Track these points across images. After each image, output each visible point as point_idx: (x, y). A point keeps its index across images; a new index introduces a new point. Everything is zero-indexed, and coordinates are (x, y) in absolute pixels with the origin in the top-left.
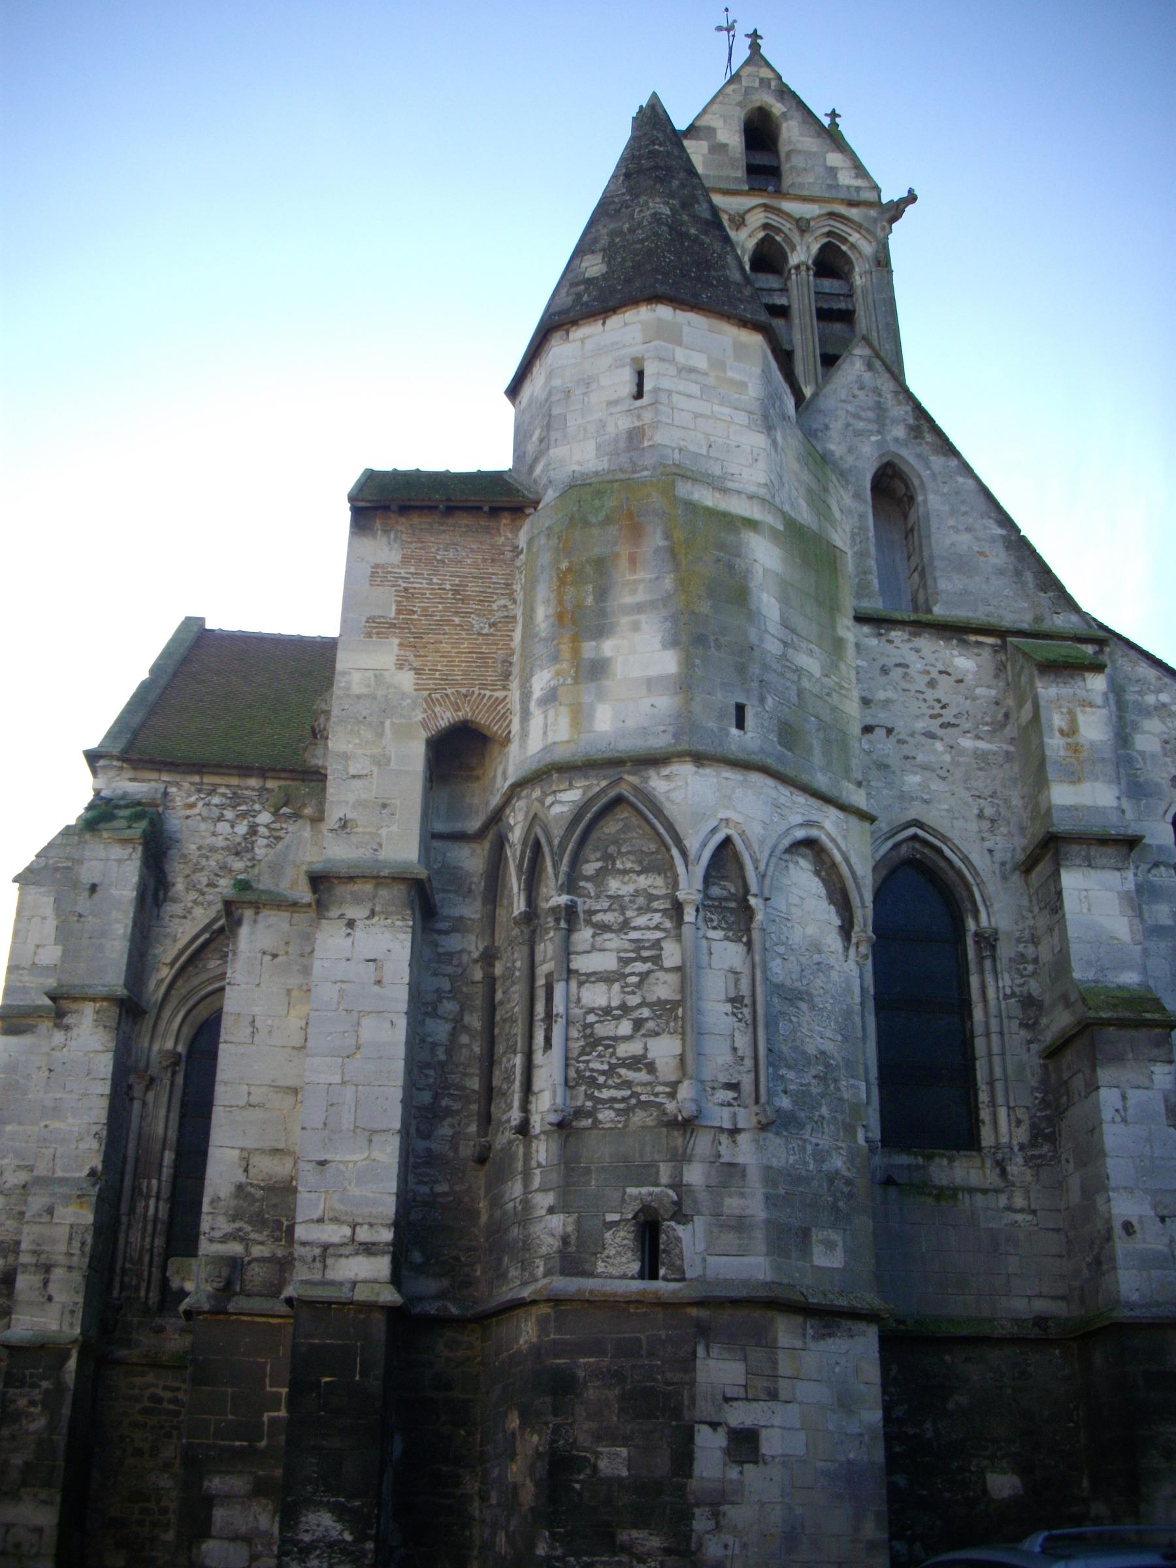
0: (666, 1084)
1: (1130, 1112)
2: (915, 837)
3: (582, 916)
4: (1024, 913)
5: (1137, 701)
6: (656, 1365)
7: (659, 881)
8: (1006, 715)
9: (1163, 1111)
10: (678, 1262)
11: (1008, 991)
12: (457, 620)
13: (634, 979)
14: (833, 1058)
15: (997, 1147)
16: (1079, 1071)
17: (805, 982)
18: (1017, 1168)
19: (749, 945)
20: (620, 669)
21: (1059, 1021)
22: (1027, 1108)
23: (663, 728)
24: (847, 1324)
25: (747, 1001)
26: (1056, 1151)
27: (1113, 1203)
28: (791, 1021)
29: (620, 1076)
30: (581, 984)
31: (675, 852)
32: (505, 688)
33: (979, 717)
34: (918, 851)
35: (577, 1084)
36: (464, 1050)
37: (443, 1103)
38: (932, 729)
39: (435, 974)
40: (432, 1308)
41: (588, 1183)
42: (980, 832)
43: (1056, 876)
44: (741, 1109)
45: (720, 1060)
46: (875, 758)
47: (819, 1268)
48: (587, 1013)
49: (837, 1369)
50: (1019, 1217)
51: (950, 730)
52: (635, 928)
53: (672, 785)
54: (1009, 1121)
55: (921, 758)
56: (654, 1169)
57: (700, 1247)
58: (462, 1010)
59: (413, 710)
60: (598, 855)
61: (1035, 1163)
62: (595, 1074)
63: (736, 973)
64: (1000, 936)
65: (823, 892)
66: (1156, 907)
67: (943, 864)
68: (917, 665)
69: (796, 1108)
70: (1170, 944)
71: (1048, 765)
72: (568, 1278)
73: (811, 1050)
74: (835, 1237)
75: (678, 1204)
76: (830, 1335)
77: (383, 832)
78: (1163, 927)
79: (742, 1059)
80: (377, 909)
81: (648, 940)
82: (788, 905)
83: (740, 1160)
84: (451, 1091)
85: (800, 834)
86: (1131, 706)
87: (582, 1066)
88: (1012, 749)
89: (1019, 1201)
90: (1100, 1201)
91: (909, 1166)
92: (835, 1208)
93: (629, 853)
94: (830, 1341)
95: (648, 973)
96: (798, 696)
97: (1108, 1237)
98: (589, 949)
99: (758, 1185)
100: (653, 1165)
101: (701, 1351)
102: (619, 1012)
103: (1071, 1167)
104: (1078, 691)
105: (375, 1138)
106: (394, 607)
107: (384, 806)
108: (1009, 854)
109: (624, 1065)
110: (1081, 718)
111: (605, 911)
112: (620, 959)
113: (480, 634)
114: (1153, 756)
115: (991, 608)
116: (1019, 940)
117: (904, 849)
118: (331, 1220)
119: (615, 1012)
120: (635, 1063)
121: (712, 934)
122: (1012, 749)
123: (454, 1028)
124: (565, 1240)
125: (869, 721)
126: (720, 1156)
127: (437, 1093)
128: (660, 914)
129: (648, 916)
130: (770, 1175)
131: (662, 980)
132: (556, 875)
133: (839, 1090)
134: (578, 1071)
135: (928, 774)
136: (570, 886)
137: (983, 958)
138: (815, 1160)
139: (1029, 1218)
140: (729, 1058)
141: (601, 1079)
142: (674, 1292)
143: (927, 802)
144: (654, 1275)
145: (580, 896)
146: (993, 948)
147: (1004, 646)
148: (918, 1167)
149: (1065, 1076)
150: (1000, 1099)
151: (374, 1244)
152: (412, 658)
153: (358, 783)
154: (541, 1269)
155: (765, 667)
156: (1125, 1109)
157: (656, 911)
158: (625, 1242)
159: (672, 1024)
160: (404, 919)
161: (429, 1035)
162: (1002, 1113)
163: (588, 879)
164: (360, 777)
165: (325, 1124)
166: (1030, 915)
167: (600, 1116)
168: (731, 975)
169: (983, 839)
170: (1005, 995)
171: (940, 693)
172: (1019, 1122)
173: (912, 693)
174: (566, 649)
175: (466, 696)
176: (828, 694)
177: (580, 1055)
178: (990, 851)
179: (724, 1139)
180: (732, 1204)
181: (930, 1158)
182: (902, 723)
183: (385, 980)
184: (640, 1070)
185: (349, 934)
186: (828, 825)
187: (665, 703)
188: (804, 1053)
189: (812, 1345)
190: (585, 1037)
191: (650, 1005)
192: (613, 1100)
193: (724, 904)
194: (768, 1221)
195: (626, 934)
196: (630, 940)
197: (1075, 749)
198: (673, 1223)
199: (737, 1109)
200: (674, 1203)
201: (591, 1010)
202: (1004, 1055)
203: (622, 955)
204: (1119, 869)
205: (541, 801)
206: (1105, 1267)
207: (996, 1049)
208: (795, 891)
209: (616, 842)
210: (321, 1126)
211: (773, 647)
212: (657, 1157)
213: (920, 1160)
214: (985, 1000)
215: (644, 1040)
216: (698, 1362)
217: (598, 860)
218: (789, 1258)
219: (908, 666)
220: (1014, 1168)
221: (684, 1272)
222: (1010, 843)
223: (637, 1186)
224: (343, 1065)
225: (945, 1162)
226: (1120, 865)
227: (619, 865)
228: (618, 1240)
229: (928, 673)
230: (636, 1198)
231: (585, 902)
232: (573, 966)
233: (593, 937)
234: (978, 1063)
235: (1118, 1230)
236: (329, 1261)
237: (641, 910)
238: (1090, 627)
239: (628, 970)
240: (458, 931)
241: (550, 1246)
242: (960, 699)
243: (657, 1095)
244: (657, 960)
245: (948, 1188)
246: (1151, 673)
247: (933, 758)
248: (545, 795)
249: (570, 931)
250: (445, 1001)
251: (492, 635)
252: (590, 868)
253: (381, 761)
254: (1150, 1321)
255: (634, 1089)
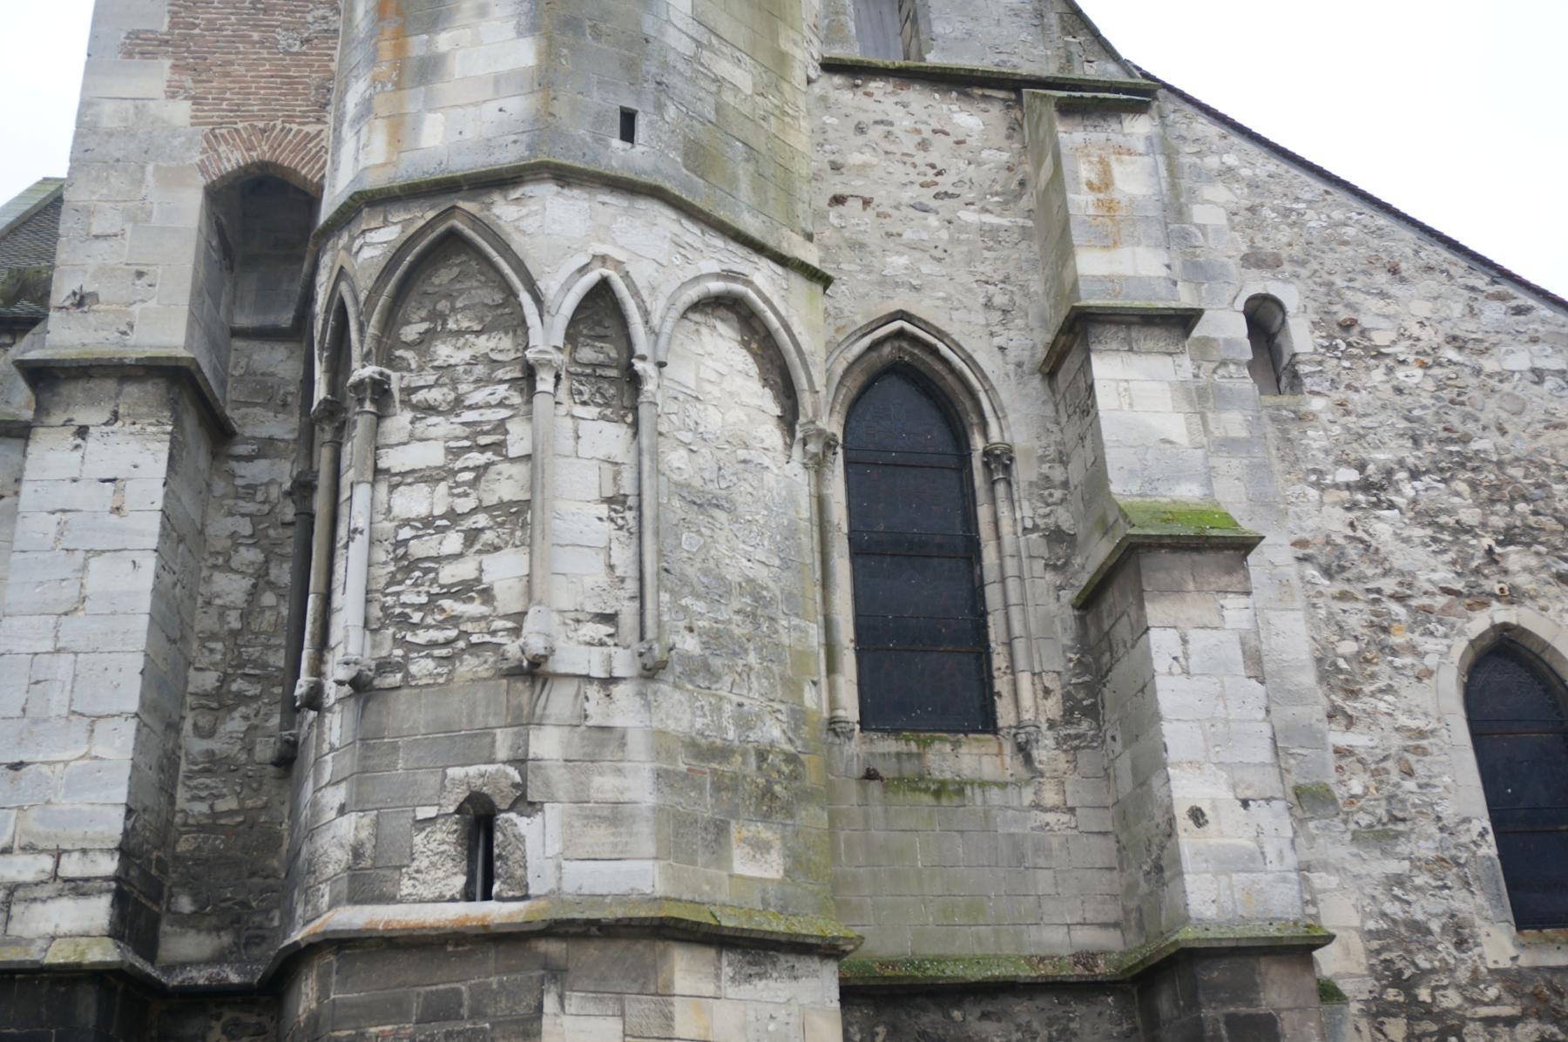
0: (506, 617)
1: (1193, 661)
2: (901, 334)
3: (397, 395)
4: (1049, 425)
5: (1195, 165)
6: (483, 1030)
7: (506, 342)
8: (1022, 184)
9: (1240, 658)
10: (519, 872)
11: (1029, 524)
12: (256, 36)
13: (468, 476)
14: (766, 588)
15: (1020, 726)
16: (1123, 614)
17: (723, 485)
18: (1046, 752)
19: (635, 426)
20: (457, 67)
21: (1099, 552)
22: (1059, 673)
23: (514, 137)
24: (785, 960)
25: (631, 501)
26: (1099, 728)
27: (1173, 783)
28: (699, 533)
29: (443, 610)
30: (393, 488)
31: (525, 298)
32: (319, 120)
33: (986, 186)
34: (905, 351)
35: (383, 626)
36: (268, 613)
37: (234, 687)
38: (924, 200)
39: (230, 514)
40: (200, 977)
41: (392, 766)
42: (988, 325)
43: (1088, 361)
44: (620, 650)
45: (589, 582)
46: (847, 234)
47: (741, 877)
48: (400, 527)
49: (771, 1027)
50: (1051, 818)
51: (947, 201)
52: (470, 407)
53: (524, 211)
54: (1035, 693)
55: (908, 235)
56: (488, 739)
57: (554, 847)
58: (267, 561)
59: (188, 149)
60: (423, 313)
61: (1072, 746)
62: (408, 610)
63: (616, 464)
64: (1017, 455)
65: (753, 369)
66: (1225, 416)
67: (939, 367)
68: (903, 122)
69: (707, 653)
70: (1245, 461)
71: (1072, 225)
72: (358, 907)
73: (732, 575)
74: (766, 833)
75: (521, 787)
76: (760, 976)
77: (136, 309)
78: (1234, 441)
79: (622, 580)
80: (121, 411)
81: (489, 422)
82: (699, 380)
83: (617, 722)
84: (247, 671)
85: (716, 286)
86: (1186, 170)
87: (390, 600)
88: (1030, 223)
89: (1050, 797)
90: (1156, 782)
91: (898, 755)
92: (767, 794)
93: (463, 309)
94: (761, 984)
95: (487, 466)
96: (717, 111)
97: (1171, 833)
98: (405, 439)
99: (643, 757)
100: (488, 732)
101: (550, 1003)
102: (445, 522)
103: (1118, 746)
104: (1112, 136)
105: (101, 726)
106: (167, 19)
107: (140, 274)
108: (1027, 353)
109: (448, 595)
110: (1117, 170)
111: (430, 387)
112: (449, 450)
113: (287, 53)
114: (1217, 230)
115: (1004, 57)
116: (1042, 459)
117: (887, 349)
118: (23, 849)
119: (439, 523)
120: (463, 591)
121: (579, 411)
122: (1030, 223)
123: (255, 586)
124: (357, 853)
125: (839, 190)
126: (586, 717)
127: (225, 674)
128: (506, 386)
129: (489, 390)
130: (661, 742)
131: (506, 475)
132: (362, 342)
133: (776, 632)
134: (384, 608)
135: (918, 255)
136: (385, 353)
137: (993, 483)
138: (737, 725)
139: (1065, 818)
140: (602, 578)
141: (416, 617)
142: (510, 915)
143: (916, 289)
144: (487, 896)
145: (395, 370)
146: (1007, 468)
147: (1019, 101)
148: (910, 755)
149: (1106, 628)
150: (1021, 663)
151: (87, 880)
152: (189, 84)
153: (103, 244)
154: (327, 898)
155: (665, 65)
156: (1186, 656)
157: (501, 382)
158: (444, 847)
159: (518, 533)
160: (159, 423)
161: (219, 596)
162: (1025, 681)
163: (408, 346)
164: (106, 237)
165: (24, 710)
166: (1055, 428)
167: (413, 669)
168: (607, 466)
169: (992, 334)
170: (1025, 529)
171: (933, 157)
172: (1047, 692)
173: (898, 156)
174: (386, 47)
175: (263, 131)
176: (764, 119)
177: (388, 585)
178: (1002, 349)
179: (593, 691)
180: (604, 785)
181: (926, 744)
182: (883, 193)
183: (126, 508)
184: (472, 599)
185: (77, 447)
186: (759, 279)
187: (518, 106)
188: (721, 578)
189: (731, 991)
190: (396, 560)
191: (487, 509)
192: (434, 644)
193: (599, 372)
194: (658, 810)
195: (458, 415)
196: (463, 424)
197: (1110, 207)
198: (512, 815)
199: (613, 649)
200: (515, 786)
201: (406, 522)
202: (1027, 611)
203: (452, 444)
204: (1170, 354)
205: (348, 248)
206: (1167, 874)
207: (1013, 598)
208: (710, 363)
209: (449, 296)
210: (18, 712)
211: (679, 44)
212: (492, 722)
213: (913, 747)
214: (998, 537)
215: (478, 558)
216: (545, 1020)
217: (423, 320)
218: (694, 863)
219: (891, 124)
220: (1044, 752)
221: (527, 886)
222: (1029, 339)
223: (463, 765)
224: (56, 627)
225: (948, 748)
226: (1172, 349)
227: (451, 325)
228: (433, 846)
229: (918, 131)
230: (461, 782)
231: (402, 378)
232: (382, 464)
233: (412, 423)
234: (990, 619)
235: (1183, 822)
236: (16, 910)
237: (480, 382)
238: (1131, 75)
239: (459, 465)
240: (265, 457)
241: (338, 861)
242: (962, 165)
243: (493, 633)
244: (497, 447)
245: (954, 782)
246: (1213, 130)
247: (925, 236)
248: (353, 239)
249: (380, 417)
250: (242, 549)
251: (305, 54)
252: (411, 332)
253: (138, 217)
254: (1233, 944)
255: (463, 628)
